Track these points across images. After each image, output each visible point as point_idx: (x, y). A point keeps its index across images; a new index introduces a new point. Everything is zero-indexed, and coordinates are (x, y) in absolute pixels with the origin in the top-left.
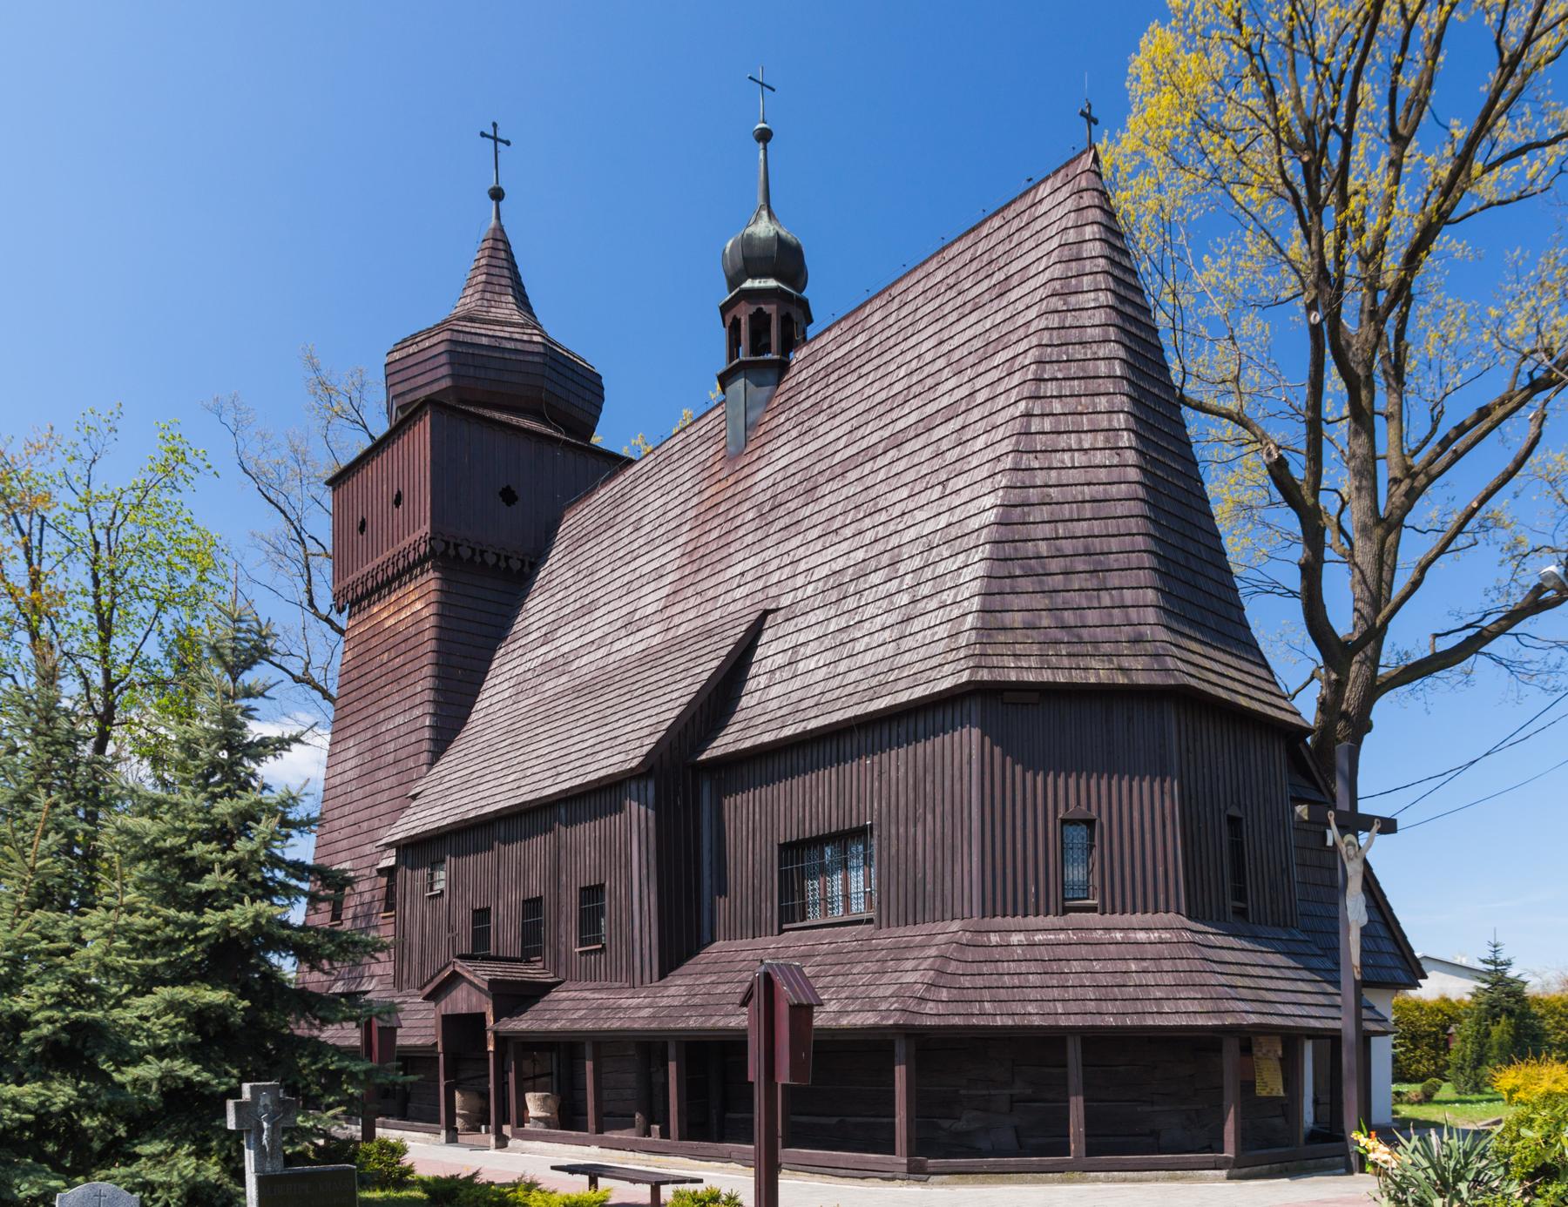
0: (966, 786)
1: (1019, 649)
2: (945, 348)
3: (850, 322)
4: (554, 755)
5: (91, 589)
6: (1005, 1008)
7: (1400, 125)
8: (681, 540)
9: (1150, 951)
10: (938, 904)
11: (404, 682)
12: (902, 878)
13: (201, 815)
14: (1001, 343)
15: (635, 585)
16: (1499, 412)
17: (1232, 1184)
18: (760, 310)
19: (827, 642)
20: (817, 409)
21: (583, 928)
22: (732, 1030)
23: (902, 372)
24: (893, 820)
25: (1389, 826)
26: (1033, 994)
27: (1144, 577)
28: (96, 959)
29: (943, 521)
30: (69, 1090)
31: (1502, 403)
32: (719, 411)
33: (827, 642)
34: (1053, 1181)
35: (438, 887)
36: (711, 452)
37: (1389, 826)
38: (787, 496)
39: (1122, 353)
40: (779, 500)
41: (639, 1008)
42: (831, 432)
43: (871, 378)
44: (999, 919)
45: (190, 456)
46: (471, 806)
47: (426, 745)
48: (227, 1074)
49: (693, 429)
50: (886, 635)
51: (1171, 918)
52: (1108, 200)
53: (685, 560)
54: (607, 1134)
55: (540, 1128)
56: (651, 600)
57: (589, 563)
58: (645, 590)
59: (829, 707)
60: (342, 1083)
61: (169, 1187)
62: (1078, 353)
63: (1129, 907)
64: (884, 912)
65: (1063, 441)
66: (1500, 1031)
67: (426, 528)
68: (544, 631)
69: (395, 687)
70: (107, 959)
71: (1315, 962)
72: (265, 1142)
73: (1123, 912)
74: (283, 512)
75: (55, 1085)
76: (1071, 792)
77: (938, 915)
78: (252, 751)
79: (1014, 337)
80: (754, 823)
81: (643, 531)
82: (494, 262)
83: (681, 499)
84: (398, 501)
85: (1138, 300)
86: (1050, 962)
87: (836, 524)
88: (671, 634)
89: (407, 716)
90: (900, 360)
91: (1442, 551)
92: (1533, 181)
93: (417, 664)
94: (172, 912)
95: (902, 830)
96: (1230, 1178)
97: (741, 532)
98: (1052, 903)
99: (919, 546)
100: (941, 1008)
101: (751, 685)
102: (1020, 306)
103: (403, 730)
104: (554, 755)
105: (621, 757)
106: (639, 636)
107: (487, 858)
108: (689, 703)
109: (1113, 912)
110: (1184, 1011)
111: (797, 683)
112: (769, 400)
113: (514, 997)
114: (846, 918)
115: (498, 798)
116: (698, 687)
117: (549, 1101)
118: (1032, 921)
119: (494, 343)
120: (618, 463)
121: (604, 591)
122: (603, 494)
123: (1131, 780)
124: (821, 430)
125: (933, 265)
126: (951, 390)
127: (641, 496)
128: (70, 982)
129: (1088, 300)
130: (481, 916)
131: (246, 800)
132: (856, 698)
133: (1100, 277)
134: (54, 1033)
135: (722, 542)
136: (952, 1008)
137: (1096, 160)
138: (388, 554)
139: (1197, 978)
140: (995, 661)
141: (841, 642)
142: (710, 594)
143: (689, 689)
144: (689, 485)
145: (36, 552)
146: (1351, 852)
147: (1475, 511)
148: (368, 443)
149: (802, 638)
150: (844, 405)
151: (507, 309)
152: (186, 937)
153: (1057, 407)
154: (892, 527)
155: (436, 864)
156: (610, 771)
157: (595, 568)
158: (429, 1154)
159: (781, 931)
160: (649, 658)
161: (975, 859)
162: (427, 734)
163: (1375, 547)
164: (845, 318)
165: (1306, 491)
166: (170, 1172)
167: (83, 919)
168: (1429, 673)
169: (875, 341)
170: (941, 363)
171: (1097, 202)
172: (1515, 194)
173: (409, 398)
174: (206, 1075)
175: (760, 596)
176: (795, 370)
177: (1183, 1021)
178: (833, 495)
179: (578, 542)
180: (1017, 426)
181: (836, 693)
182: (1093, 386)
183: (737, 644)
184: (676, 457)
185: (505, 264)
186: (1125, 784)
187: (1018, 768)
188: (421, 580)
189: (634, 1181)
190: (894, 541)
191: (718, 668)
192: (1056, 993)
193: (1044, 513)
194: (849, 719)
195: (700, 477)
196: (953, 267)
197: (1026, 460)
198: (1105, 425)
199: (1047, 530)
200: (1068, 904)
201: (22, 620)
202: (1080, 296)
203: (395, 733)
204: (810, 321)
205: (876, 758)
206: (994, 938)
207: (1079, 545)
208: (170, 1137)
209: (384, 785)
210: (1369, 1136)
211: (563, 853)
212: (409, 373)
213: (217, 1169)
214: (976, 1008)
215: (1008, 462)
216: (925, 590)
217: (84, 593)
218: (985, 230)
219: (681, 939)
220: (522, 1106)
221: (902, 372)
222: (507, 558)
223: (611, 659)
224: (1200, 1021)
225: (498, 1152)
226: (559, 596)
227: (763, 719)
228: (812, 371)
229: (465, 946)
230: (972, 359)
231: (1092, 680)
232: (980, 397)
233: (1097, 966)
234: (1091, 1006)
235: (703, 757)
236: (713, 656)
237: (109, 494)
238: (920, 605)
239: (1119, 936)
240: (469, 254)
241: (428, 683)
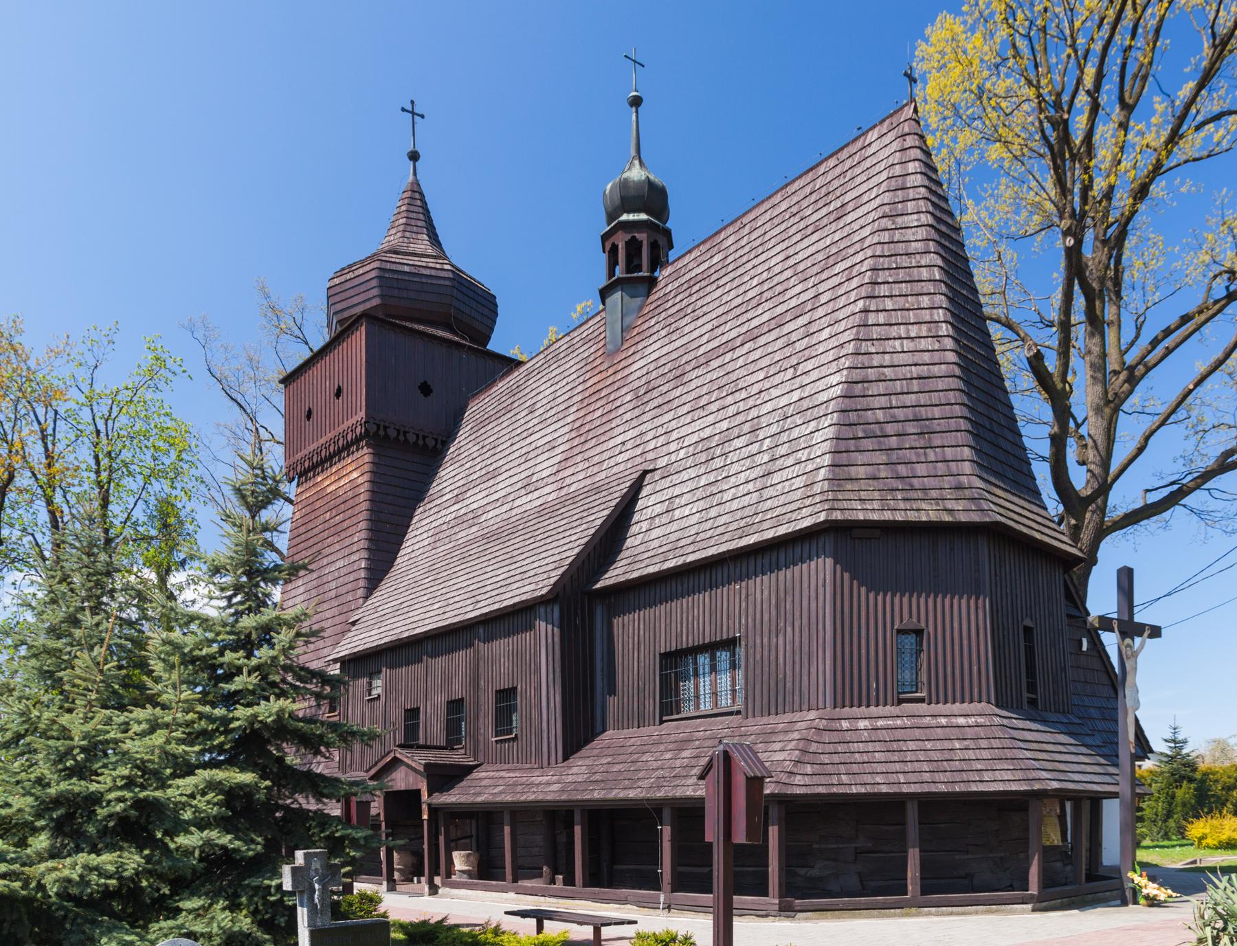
0: (821, 605)
1: (863, 495)
2: (791, 261)
3: (708, 245)
4: (472, 588)
5: (95, 467)
6: (858, 779)
7: (1127, 95)
8: (569, 419)
9: (970, 733)
10: (797, 698)
11: (343, 535)
12: (765, 678)
13: (228, 629)
14: (840, 256)
15: (532, 455)
16: (1199, 319)
17: (1038, 915)
18: (634, 237)
19: (699, 494)
20: (682, 314)
21: (498, 722)
22: (631, 800)
23: (755, 282)
24: (758, 632)
25: (1156, 632)
26: (880, 768)
27: (961, 438)
28: (160, 747)
29: (795, 396)
30: (137, 858)
31: (1200, 312)
32: (598, 318)
33: (699, 494)
34: (894, 916)
35: (375, 693)
36: (592, 350)
37: (1156, 632)
38: (659, 382)
39: (940, 262)
40: (652, 384)
41: (548, 784)
42: (696, 332)
43: (728, 288)
44: (847, 709)
45: (170, 363)
46: (403, 629)
47: (362, 583)
48: (253, 841)
49: (576, 334)
50: (751, 487)
51: (983, 706)
52: (925, 142)
53: (573, 434)
54: (520, 883)
55: (464, 879)
56: (545, 466)
57: (492, 439)
58: (540, 459)
59: (704, 544)
60: (344, 848)
61: (209, 936)
62: (905, 261)
63: (950, 698)
64: (750, 706)
65: (894, 331)
66: (1184, 792)
67: (362, 414)
68: (455, 492)
69: (336, 538)
70: (168, 748)
71: (1089, 740)
72: (316, 901)
73: (946, 702)
74: (241, 406)
75: (126, 854)
76: (904, 608)
77: (796, 707)
78: (270, 576)
79: (851, 251)
80: (638, 637)
81: (537, 413)
82: (412, 208)
83: (568, 387)
84: (338, 393)
85: (950, 221)
86: (893, 744)
87: (703, 402)
88: (564, 492)
89: (346, 561)
90: (752, 273)
91: (1163, 423)
92: (1218, 144)
93: (354, 520)
94: (208, 709)
95: (766, 640)
96: (1034, 910)
97: (621, 411)
98: (889, 696)
99: (776, 416)
100: (807, 780)
101: (634, 529)
102: (855, 226)
103: (343, 571)
104: (472, 588)
105: (532, 587)
106: (536, 494)
107: (418, 669)
108: (586, 544)
109: (938, 703)
110: (1001, 780)
111: (675, 526)
112: (641, 308)
113: (443, 777)
114: (715, 711)
115: (427, 622)
116: (593, 531)
117: (472, 858)
118: (856, 711)
119: (413, 270)
120: (512, 364)
121: (504, 461)
122: (502, 386)
123: (952, 598)
124: (686, 330)
125: (778, 197)
126: (798, 294)
127: (534, 386)
128: (138, 768)
129: (912, 220)
130: (412, 714)
131: (268, 615)
132: (726, 537)
133: (921, 203)
134: (125, 810)
135: (605, 419)
136: (816, 780)
137: (916, 111)
138: (330, 435)
139: (1009, 753)
140: (845, 504)
141: (711, 493)
142: (596, 459)
143: (586, 533)
144: (574, 376)
145: (50, 438)
146: (1129, 653)
147: (1191, 391)
148: (308, 354)
150: (705, 309)
151: (422, 244)
152: (217, 729)
153: (889, 304)
154: (751, 402)
155: (374, 674)
156: (524, 598)
157: (497, 443)
158: (404, 905)
159: (662, 722)
160: (546, 511)
161: (828, 662)
162: (363, 574)
163: (1105, 423)
166: (209, 924)
167: (131, 716)
168: (1137, 522)
169: (731, 259)
170: (788, 273)
171: (917, 144)
172: (1206, 153)
173: (346, 314)
174: (237, 843)
175: (639, 460)
176: (662, 284)
177: (1000, 787)
178: (698, 380)
179: (483, 423)
180: (857, 320)
181: (709, 534)
182: (917, 287)
183: (623, 497)
184: (562, 355)
185: (421, 210)
186: (947, 601)
187: (863, 590)
188: (356, 455)
189: (581, 924)
190: (754, 413)
191: (609, 516)
192: (898, 767)
194: (724, 553)
195: (584, 370)
196: (795, 199)
197: (866, 347)
198: (928, 318)
199: (883, 401)
200: (902, 696)
201: (39, 491)
202: (906, 218)
203: (336, 574)
204: (671, 247)
205: (744, 584)
206: (845, 725)
207: (909, 413)
208: (206, 894)
209: (328, 614)
210: (1141, 876)
211: (481, 663)
212: (347, 294)
213: (248, 920)
214: (835, 780)
215: (850, 348)
216: (783, 450)
217: (88, 469)
218: (822, 169)
219: (580, 729)
220: (450, 862)
221: (755, 282)
222: (424, 437)
223: (514, 512)
224: (1014, 787)
225: (431, 898)
226: (468, 466)
227: (646, 555)
228: (676, 284)
229: (400, 738)
230: (816, 269)
231: (924, 519)
232: (823, 299)
233: (929, 745)
234: (927, 777)
235: (598, 586)
236: (603, 507)
237: (108, 392)
238: (779, 463)
239: (943, 721)
240: (391, 202)
241: (364, 535)
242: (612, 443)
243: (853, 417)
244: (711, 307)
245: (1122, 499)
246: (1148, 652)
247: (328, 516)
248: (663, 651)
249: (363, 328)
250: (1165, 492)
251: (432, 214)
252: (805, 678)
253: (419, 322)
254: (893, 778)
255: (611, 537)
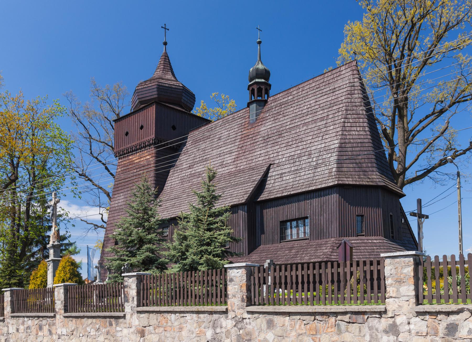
3: (286, 93)
10: (327, 234)
14: (335, 104)
23: (305, 108)
25: (427, 217)
37: (427, 217)
42: (285, 121)
56: (229, 159)
58: (226, 156)
65: (353, 129)
76: (359, 210)
77: (327, 237)
80: (271, 217)
82: (165, 62)
84: (142, 127)
95: (317, 217)
114: (298, 239)
124: (281, 119)
125: (311, 82)
140: (342, 179)
147: (432, 143)
149: (283, 171)
151: (169, 76)
153: (351, 121)
159: (280, 242)
164: (285, 91)
165: (390, 135)
176: (270, 103)
180: (342, 124)
183: (265, 172)
188: (148, 150)
192: (359, 254)
193: (350, 145)
197: (345, 133)
198: (362, 125)
212: (144, 92)
215: (340, 133)
233: (367, 248)
234: (368, 256)
235: (259, 200)
239: (370, 241)
240: (158, 61)
242: (256, 154)
243: (342, 153)
244: (290, 113)
245: (410, 174)
246: (426, 223)
247: (135, 171)
248: (281, 220)
249: (154, 106)
250: (422, 172)
251: (172, 65)
252: (330, 229)
253: (165, 102)
254: (359, 257)
255: (261, 186)
